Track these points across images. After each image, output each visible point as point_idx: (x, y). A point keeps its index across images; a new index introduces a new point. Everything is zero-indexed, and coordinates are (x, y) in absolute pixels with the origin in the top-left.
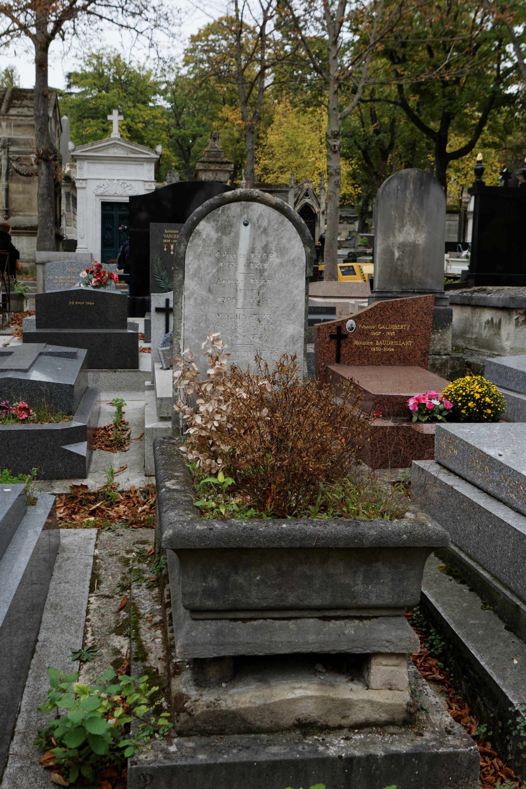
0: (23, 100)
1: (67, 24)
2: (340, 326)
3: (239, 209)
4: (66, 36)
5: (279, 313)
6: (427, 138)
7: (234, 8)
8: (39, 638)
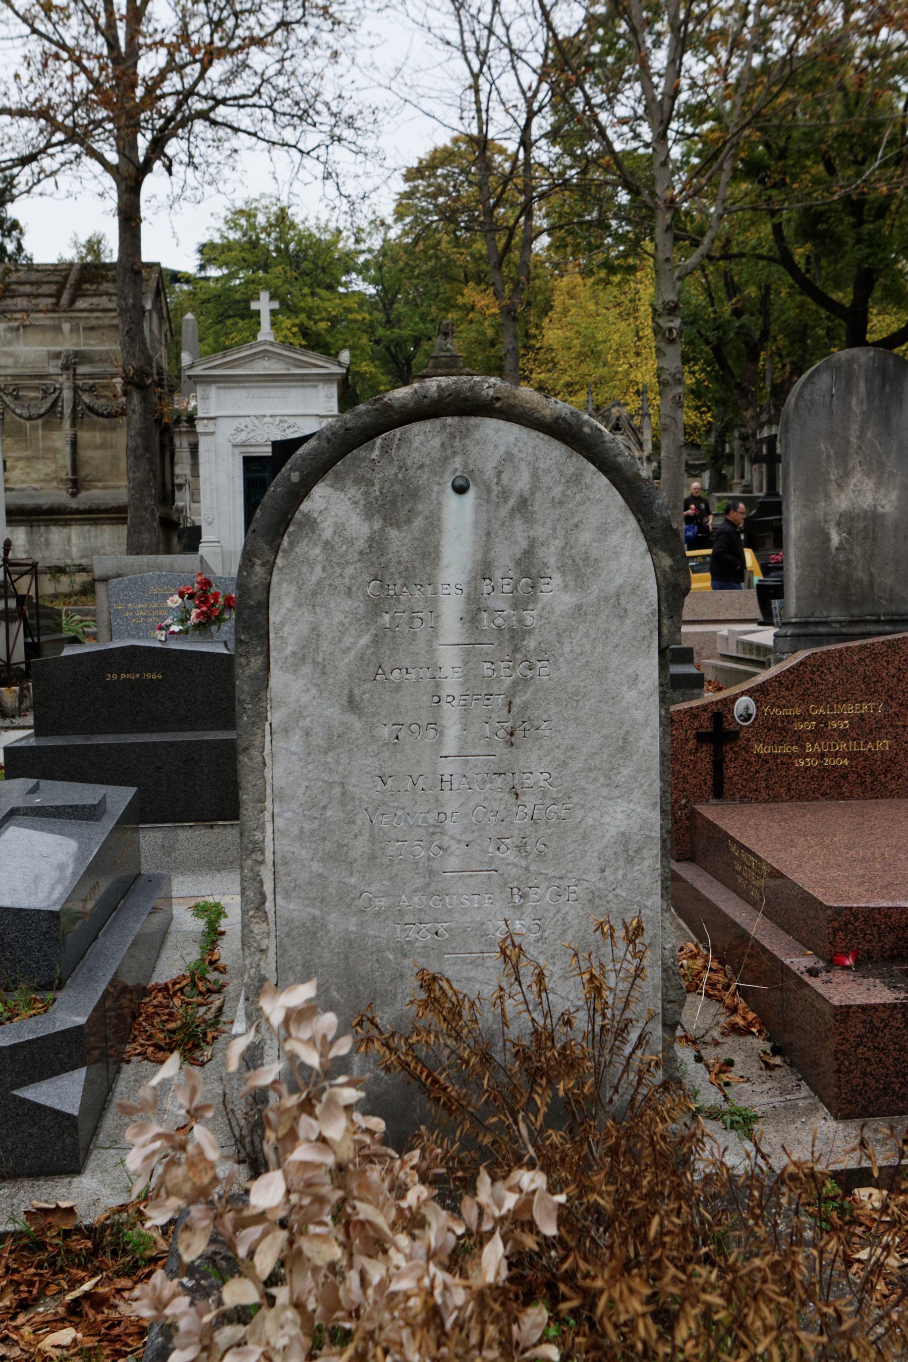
0: (100, 283)
1: (173, 147)
2: (719, 714)
3: (436, 442)
4: (176, 168)
5: (577, 765)
6: (828, 318)
7: (473, 99)
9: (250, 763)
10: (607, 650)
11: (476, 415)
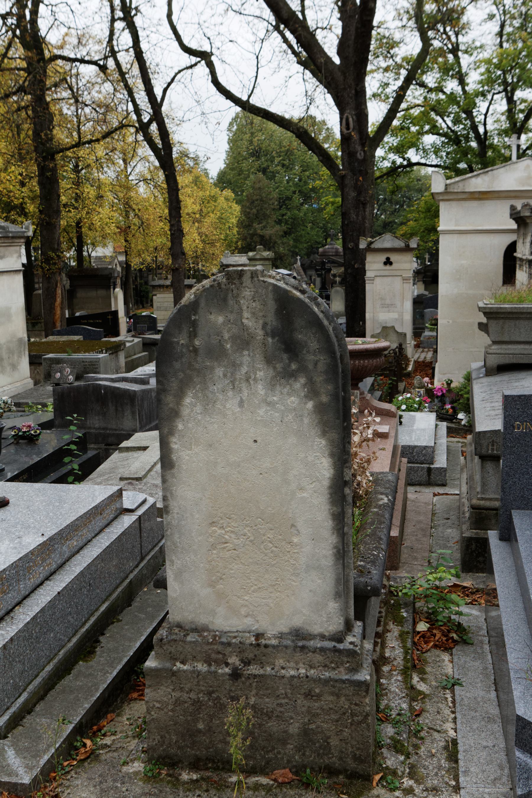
8: (495, 692)
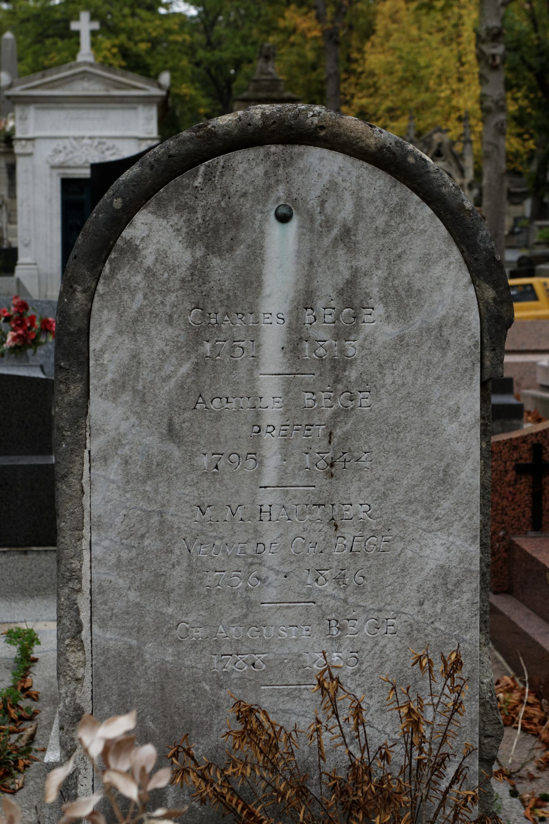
3: (260, 171)
9: (68, 491)
10: (429, 382)
11: (300, 144)
